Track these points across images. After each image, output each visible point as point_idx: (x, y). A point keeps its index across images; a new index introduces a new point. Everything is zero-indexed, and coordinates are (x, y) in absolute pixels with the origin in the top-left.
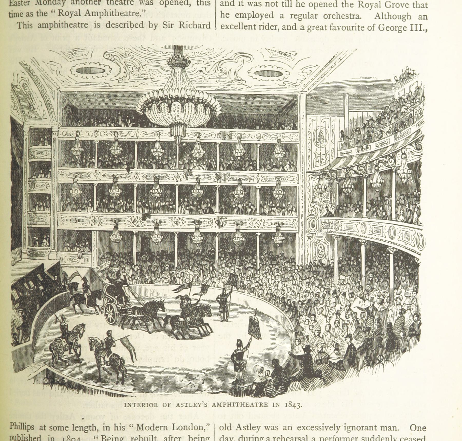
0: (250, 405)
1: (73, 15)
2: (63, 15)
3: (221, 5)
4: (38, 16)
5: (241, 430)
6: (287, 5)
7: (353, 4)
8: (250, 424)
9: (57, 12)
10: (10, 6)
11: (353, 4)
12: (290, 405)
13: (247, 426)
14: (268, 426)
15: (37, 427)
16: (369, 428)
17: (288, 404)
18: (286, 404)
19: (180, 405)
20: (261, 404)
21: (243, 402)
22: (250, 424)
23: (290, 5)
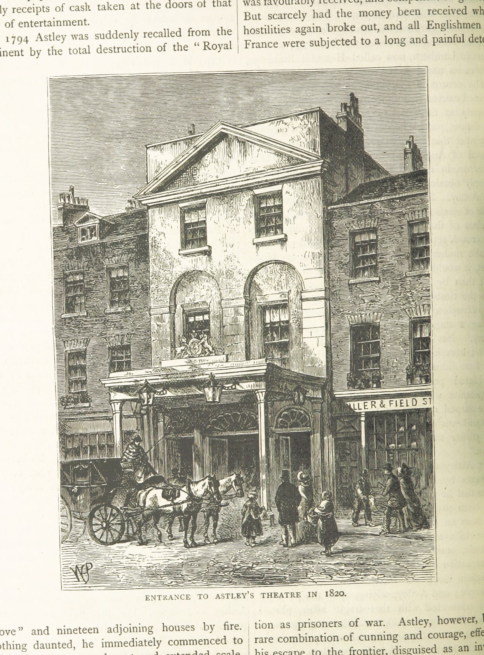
0: (279, 595)
1: (222, 48)
2: (210, 49)
3: (385, 29)
4: (49, 55)
5: (405, 625)
6: (267, 32)
7: (354, 27)
8: (416, 618)
9: (202, 46)
10: (429, 28)
11: (354, 27)
12: (332, 595)
13: (413, 620)
14: (454, 618)
15: (345, 624)
16: (37, 632)
17: (329, 593)
18: (327, 592)
19: (221, 597)
20: (292, 595)
21: (269, 592)
22: (416, 618)
23: (417, 27)
